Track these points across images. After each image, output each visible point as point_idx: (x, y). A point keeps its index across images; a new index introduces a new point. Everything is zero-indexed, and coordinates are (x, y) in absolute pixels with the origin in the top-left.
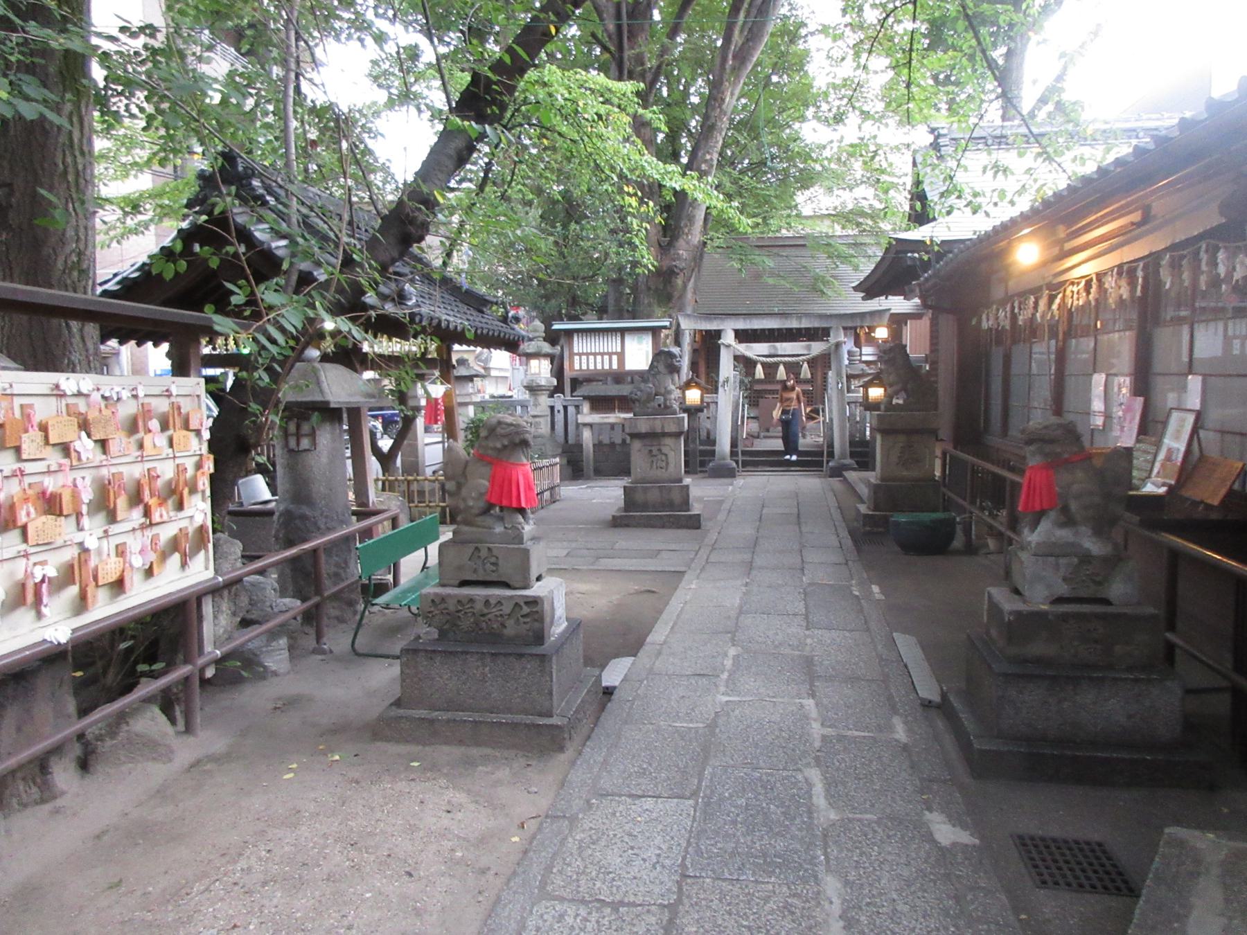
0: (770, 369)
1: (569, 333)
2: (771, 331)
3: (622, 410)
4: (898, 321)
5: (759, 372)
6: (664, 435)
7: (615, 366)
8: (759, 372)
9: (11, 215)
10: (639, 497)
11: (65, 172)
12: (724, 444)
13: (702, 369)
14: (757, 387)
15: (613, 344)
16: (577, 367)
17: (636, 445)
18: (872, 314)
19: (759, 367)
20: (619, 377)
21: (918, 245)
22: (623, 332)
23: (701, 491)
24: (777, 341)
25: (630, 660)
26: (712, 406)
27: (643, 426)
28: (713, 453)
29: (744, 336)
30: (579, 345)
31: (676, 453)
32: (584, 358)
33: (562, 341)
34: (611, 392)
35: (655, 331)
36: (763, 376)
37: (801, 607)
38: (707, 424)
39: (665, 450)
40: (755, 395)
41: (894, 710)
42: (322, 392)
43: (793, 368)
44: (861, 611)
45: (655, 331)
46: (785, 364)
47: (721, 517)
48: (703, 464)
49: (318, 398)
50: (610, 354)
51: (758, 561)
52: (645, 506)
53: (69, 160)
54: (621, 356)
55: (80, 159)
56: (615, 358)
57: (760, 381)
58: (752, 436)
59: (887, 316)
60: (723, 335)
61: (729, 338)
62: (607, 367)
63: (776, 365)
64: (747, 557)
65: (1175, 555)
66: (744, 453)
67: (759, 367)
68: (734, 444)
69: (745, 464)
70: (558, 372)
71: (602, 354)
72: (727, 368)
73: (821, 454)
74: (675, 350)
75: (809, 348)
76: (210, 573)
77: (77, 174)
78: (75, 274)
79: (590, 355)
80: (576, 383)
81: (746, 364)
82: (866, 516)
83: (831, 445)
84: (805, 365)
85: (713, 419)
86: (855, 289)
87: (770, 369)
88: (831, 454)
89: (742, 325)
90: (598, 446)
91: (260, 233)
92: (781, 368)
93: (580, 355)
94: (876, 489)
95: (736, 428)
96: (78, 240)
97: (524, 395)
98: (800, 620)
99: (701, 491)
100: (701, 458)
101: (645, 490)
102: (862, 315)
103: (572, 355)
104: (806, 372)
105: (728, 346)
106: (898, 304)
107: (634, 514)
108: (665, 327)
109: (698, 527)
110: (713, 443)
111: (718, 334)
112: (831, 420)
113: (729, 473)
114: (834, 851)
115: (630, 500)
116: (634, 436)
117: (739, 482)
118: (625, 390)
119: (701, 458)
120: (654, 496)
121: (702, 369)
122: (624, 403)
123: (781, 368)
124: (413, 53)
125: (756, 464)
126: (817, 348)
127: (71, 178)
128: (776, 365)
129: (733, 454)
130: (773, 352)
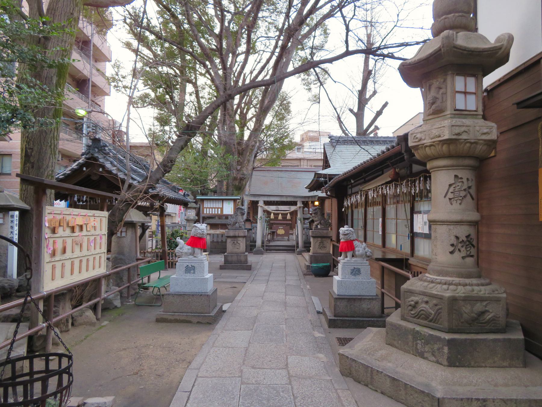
0: (276, 215)
1: (202, 200)
2: (277, 202)
3: (221, 229)
4: (322, 200)
5: (272, 216)
6: (239, 237)
7: (219, 213)
8: (272, 216)
9: (31, 158)
10: (230, 259)
11: (51, 146)
12: (259, 243)
13: (251, 215)
14: (271, 222)
15: (219, 205)
16: (205, 212)
17: (229, 240)
18: (312, 197)
19: (272, 214)
20: (221, 216)
21: (325, 176)
22: (223, 200)
23: (252, 259)
24: (279, 205)
25: (230, 304)
26: (255, 228)
27: (231, 233)
28: (255, 246)
29: (267, 203)
30: (206, 204)
31: (242, 244)
32: (214, 209)
33: (199, 203)
34: (216, 222)
35: (235, 200)
36: (217, 33)
37: (284, 290)
38: (253, 235)
39: (239, 242)
40: (271, 225)
41: (309, 313)
42: (131, 218)
43: (284, 215)
44: (303, 291)
45: (235, 200)
46: (282, 214)
47: (258, 267)
48: (251, 250)
49: (130, 220)
50: (218, 208)
51: (270, 279)
52: (231, 263)
53: (53, 141)
54: (222, 209)
55: (56, 142)
56: (219, 209)
57: (272, 220)
58: (269, 241)
59: (317, 197)
60: (259, 202)
61: (261, 204)
62: (216, 213)
63: (278, 214)
64: (267, 278)
65: (383, 268)
66: (266, 246)
67: (272, 214)
68: (263, 243)
69: (267, 250)
70: (198, 214)
71: (215, 208)
72: (260, 213)
73: (294, 246)
74: (243, 207)
75: (290, 208)
76: (105, 271)
77: (54, 146)
78: (50, 177)
79: (210, 208)
80: (204, 219)
81: (265, 211)
82: (307, 266)
83: (298, 243)
84: (289, 214)
85: (255, 233)
86: (306, 188)
87: (276, 215)
88: (298, 247)
89: (266, 199)
90: (212, 242)
91: (108, 165)
92: (280, 215)
93: (207, 208)
94: (311, 257)
95: (263, 236)
96: (52, 166)
97: (184, 223)
98: (284, 294)
99: (252, 259)
100: (251, 247)
101: (232, 256)
102: (309, 197)
103: (203, 208)
104: (289, 217)
105: (261, 207)
106: (320, 194)
107: (227, 265)
108: (238, 199)
109: (250, 270)
110: (255, 242)
111: (257, 202)
112: (298, 234)
113: (262, 253)
114: (288, 338)
115: (226, 261)
116: (228, 237)
117: (264, 256)
118: (223, 221)
119: (251, 247)
120: (235, 258)
121: (251, 215)
122: (224, 226)
123: (280, 215)
124: (147, 96)
125: (270, 250)
126: (293, 208)
127: (52, 147)
128: (287, 214)
129: (263, 246)
130: (277, 209)
